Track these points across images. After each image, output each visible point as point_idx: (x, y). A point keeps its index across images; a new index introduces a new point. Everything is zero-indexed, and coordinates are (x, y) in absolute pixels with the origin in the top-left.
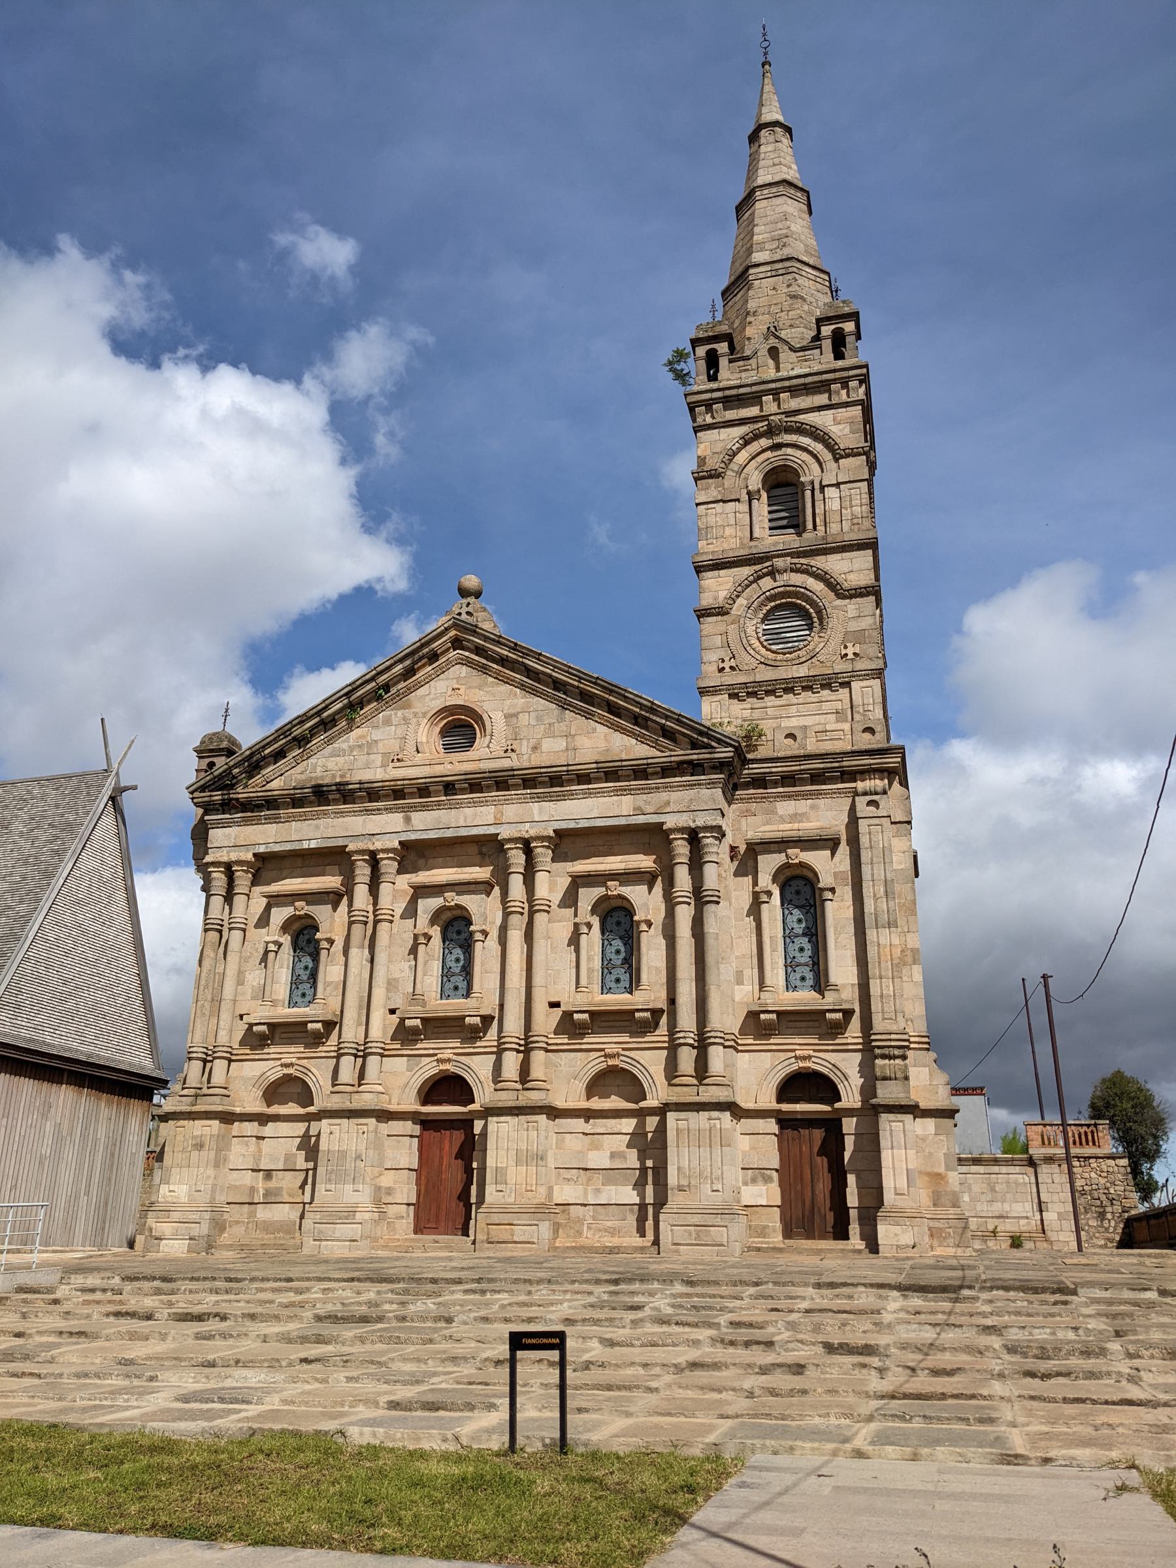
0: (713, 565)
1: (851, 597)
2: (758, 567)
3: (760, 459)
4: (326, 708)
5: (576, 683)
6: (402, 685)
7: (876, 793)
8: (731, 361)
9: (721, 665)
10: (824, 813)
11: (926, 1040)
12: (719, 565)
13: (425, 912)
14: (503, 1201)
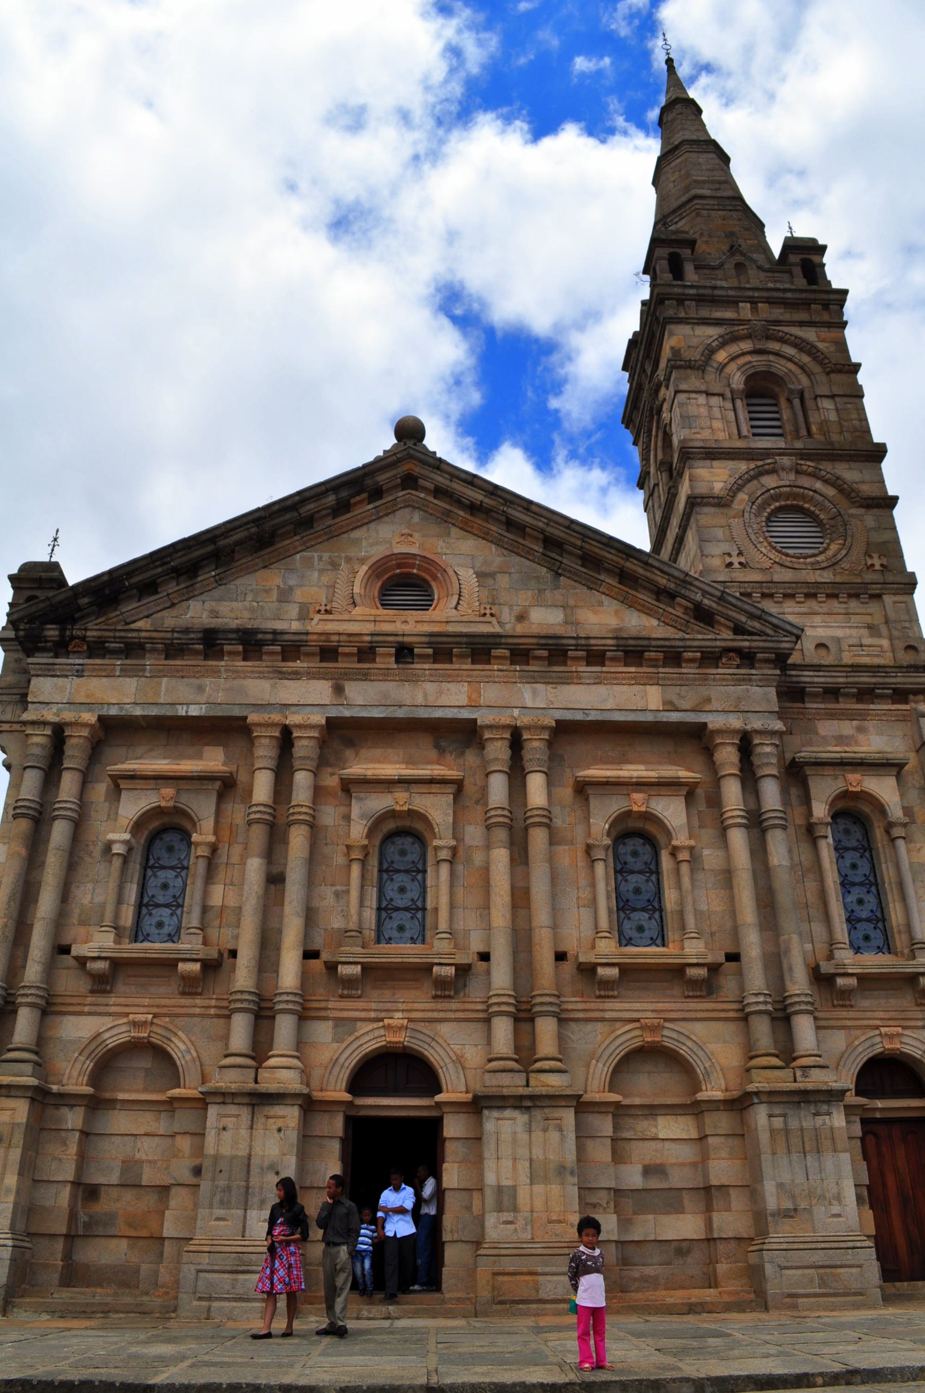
0: (706, 453)
2: (760, 463)
5: (579, 543)
9: (728, 560)
13: (362, 816)
14: (515, 1238)
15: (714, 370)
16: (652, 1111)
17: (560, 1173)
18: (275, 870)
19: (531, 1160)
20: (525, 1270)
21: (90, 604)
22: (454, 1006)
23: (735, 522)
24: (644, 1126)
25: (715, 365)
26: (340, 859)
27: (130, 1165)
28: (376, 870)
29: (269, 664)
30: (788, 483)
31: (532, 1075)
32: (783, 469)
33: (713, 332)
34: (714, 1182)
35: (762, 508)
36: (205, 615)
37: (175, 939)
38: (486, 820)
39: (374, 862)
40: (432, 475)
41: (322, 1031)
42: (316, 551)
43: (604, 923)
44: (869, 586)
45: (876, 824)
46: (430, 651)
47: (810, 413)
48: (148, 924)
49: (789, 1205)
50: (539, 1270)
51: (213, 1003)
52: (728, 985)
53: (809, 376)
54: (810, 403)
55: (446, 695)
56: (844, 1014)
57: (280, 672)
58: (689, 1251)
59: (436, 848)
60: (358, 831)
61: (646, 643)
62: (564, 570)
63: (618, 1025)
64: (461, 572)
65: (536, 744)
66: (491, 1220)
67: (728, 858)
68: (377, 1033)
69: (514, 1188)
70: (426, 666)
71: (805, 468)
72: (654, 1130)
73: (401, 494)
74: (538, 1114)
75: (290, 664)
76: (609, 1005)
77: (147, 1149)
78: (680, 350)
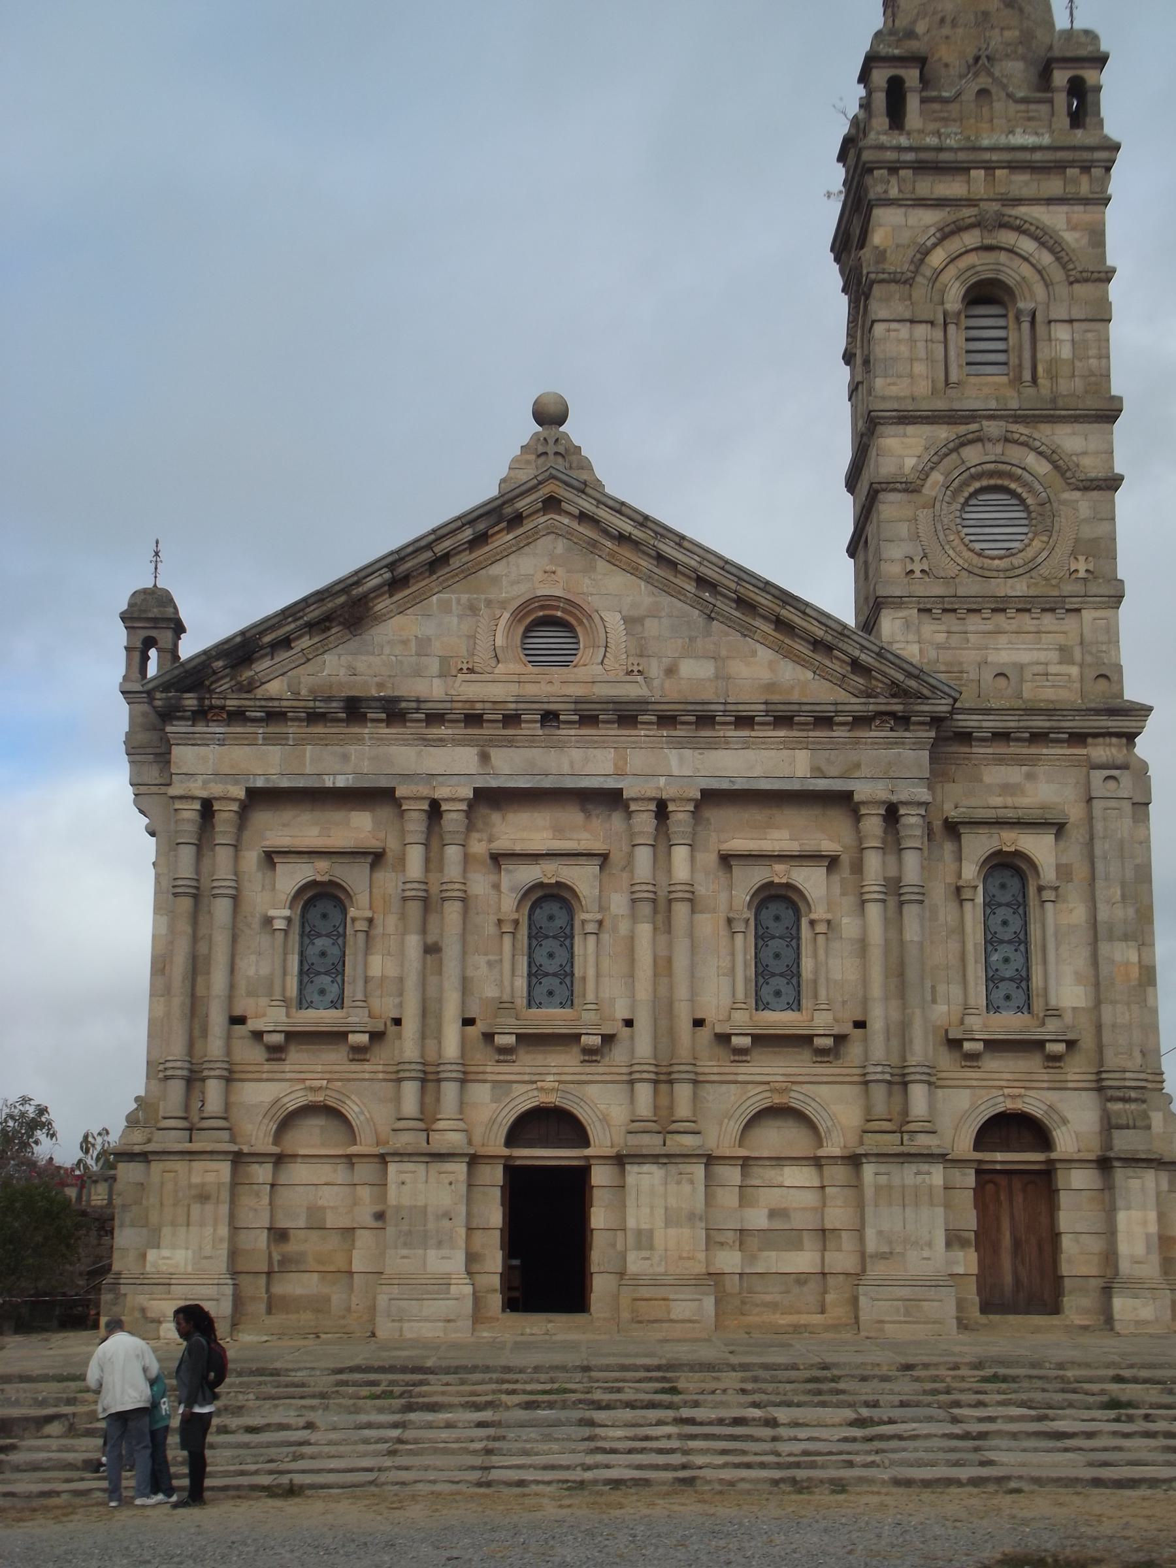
0: (899, 418)
1: (1086, 489)
2: (962, 429)
3: (963, 263)
4: (357, 583)
5: (733, 586)
6: (465, 557)
7: (1117, 768)
8: (923, 101)
10: (1048, 785)
11: (423, 887)
12: (905, 418)
13: (512, 889)
14: (651, 1271)
15: (926, 282)
16: (779, 1161)
17: (690, 1219)
18: (431, 939)
19: (666, 1209)
20: (659, 1296)
21: (225, 667)
22: (601, 1070)
23: (924, 515)
24: (771, 1174)
25: (928, 273)
26: (491, 929)
27: (314, 1211)
28: (526, 938)
29: (413, 731)
30: (993, 458)
31: (669, 1136)
32: (989, 440)
33: (930, 218)
34: (828, 1226)
35: (956, 493)
36: (342, 672)
37: (338, 1005)
38: (632, 893)
39: (524, 931)
40: (577, 500)
41: (481, 1093)
42: (453, 593)
43: (740, 995)
44: (1067, 600)
45: (1031, 882)
46: (576, 718)
47: (1040, 345)
48: (766, 992)
49: (886, 1249)
50: (671, 1297)
51: (380, 1068)
52: (854, 1051)
53: (1047, 286)
54: (1041, 329)
55: (591, 761)
56: (973, 1075)
57: (425, 740)
58: (805, 1282)
59: (583, 922)
60: (509, 904)
61: (796, 707)
62: (718, 613)
63: (750, 1086)
64: (607, 616)
65: (680, 816)
66: (631, 1256)
67: (864, 928)
68: (531, 1094)
69: (651, 1231)
70: (572, 732)
71: (1016, 436)
72: (780, 1179)
73: (542, 519)
74: (673, 1169)
75: (435, 731)
76: (742, 1069)
77: (328, 1197)
78: (885, 251)
